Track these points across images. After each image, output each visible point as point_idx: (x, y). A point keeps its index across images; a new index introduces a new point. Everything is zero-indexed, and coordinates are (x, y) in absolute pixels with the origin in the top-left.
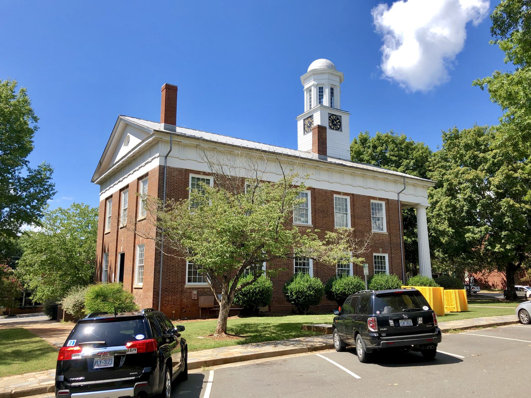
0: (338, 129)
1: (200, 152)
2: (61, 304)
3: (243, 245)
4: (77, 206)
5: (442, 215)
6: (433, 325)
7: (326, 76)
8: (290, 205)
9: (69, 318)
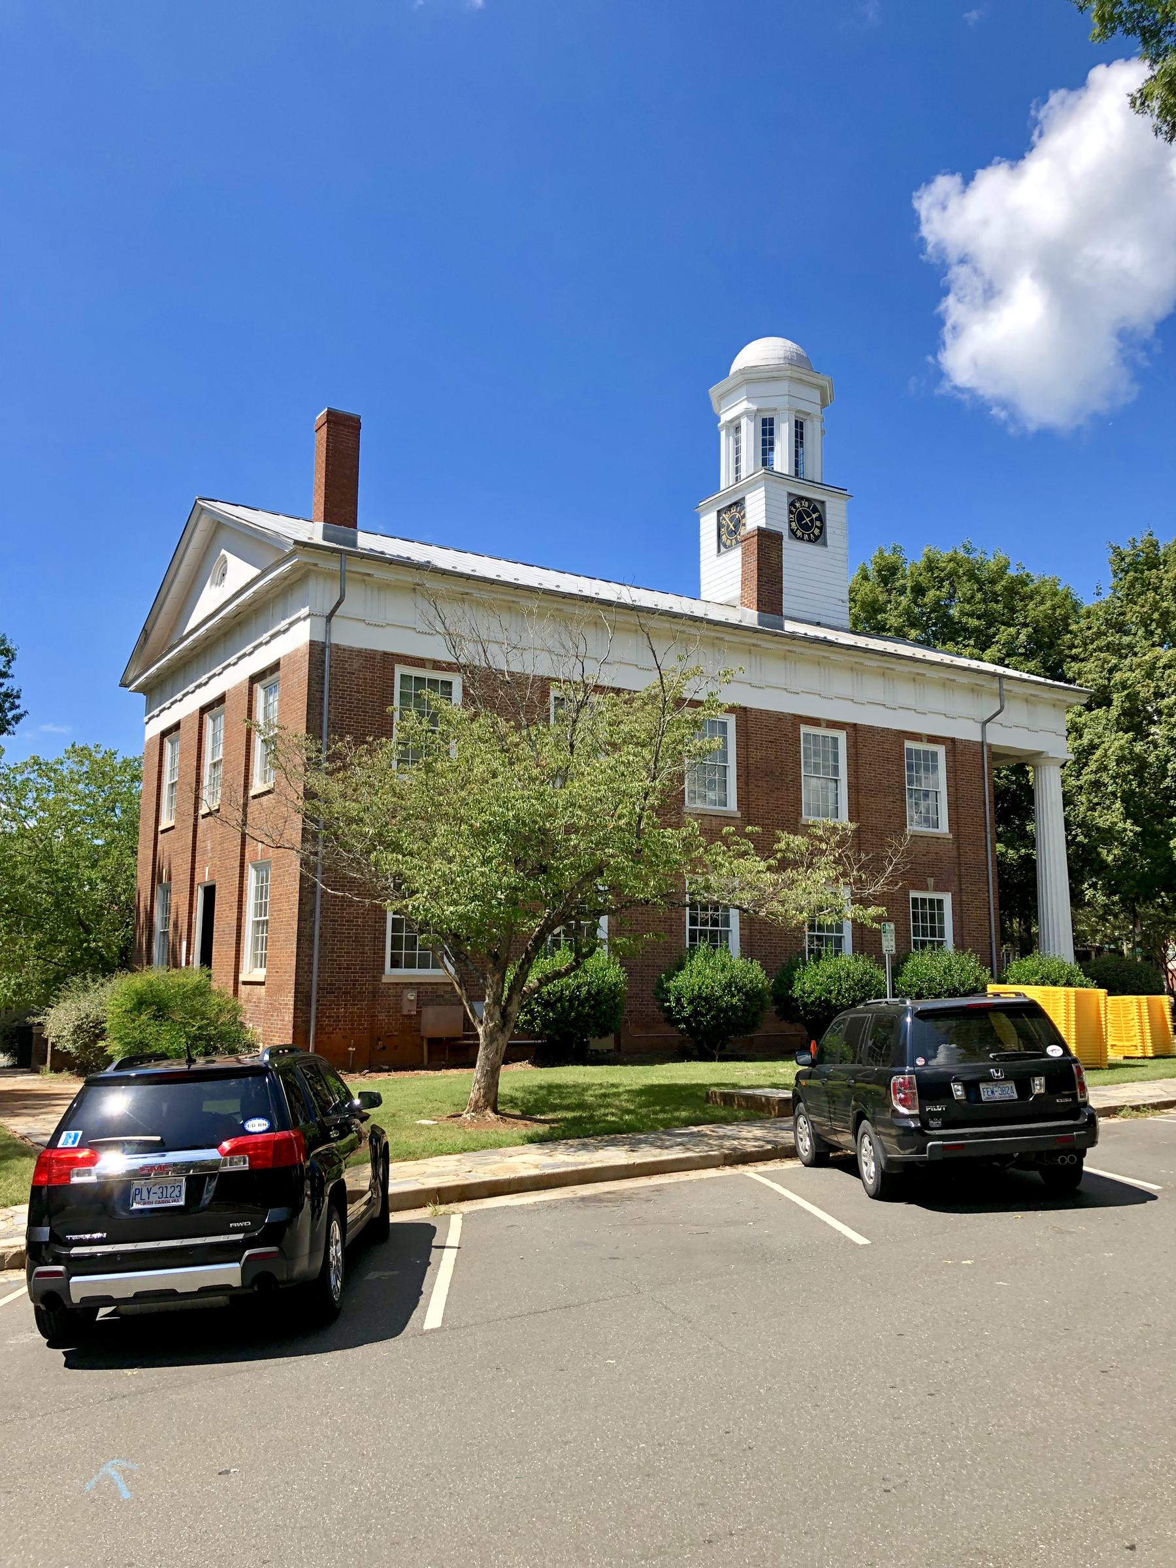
1: (424, 605)
2: (40, 1024)
3: (544, 869)
4: (82, 753)
5: (1105, 785)
6: (1074, 1096)
7: (784, 387)
8: (677, 758)
9: (63, 1062)
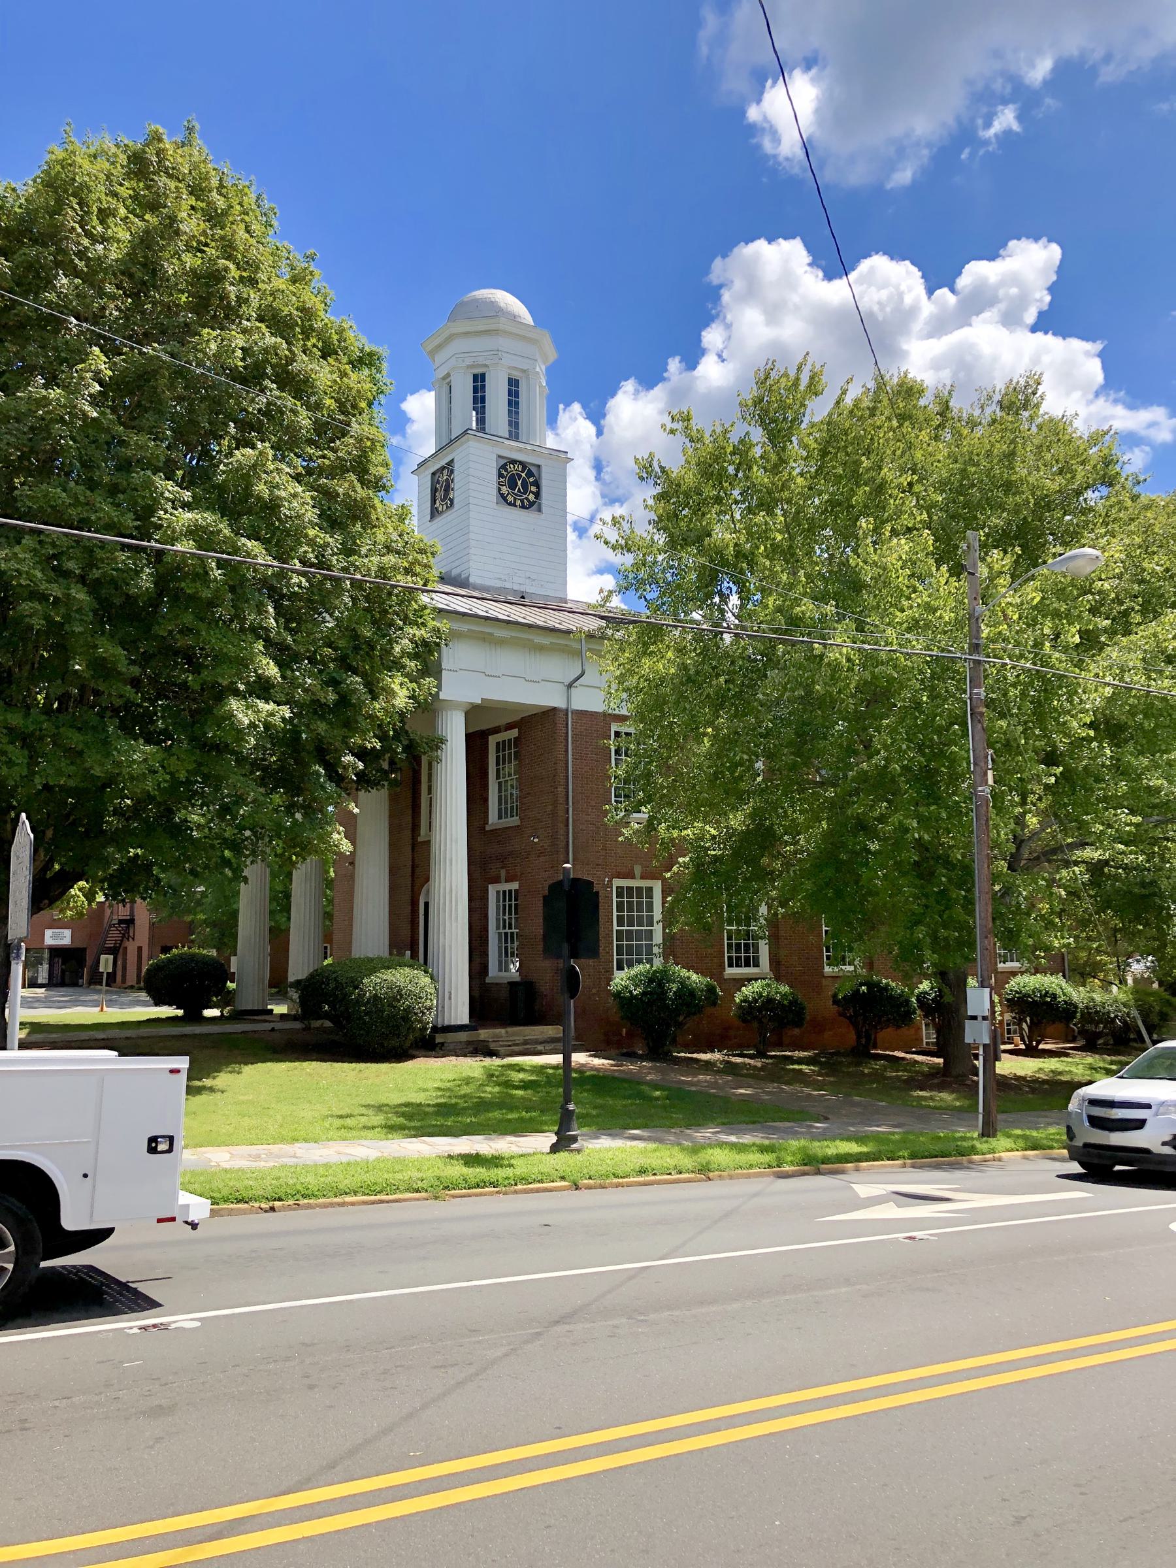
0: (526, 506)
